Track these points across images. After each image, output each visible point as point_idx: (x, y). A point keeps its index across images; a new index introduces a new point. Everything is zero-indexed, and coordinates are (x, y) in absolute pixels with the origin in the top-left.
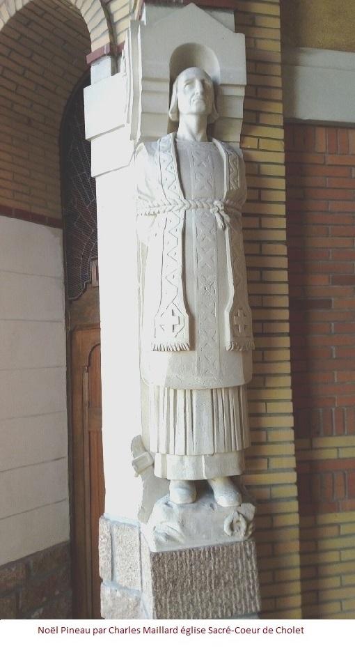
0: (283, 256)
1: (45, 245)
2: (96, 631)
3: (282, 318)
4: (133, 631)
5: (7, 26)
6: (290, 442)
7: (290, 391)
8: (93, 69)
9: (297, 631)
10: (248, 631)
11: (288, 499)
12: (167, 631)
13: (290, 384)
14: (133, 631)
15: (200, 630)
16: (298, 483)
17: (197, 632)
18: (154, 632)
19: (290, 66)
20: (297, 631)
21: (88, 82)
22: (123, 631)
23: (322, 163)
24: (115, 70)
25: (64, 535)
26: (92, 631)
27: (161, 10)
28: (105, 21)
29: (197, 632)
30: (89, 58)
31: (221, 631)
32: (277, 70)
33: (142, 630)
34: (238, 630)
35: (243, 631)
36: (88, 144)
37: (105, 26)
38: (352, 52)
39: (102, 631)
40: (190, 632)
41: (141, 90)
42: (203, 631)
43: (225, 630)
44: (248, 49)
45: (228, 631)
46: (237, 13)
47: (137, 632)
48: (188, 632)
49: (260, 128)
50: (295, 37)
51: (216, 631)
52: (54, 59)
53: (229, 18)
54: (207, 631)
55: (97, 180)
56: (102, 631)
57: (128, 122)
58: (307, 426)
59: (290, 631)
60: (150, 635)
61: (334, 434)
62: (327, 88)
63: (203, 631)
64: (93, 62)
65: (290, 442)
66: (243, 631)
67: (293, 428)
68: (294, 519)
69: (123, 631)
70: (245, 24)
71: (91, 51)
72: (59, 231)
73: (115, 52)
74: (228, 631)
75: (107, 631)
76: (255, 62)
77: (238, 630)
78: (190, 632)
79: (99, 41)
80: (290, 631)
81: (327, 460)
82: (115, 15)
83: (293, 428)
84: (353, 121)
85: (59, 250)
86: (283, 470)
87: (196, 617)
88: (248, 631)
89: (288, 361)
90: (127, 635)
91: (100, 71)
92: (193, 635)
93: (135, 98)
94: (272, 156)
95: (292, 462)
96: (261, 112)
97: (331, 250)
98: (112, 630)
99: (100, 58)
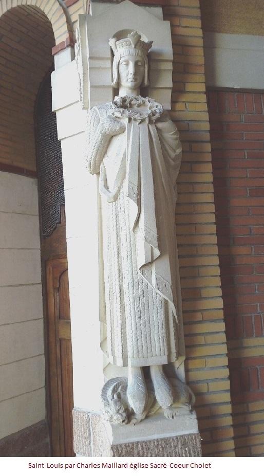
0: (211, 223)
1: (24, 189)
2: (68, 466)
3: (207, 160)
4: (95, 466)
6: (226, 391)
7: (218, 269)
8: (56, 57)
9: (206, 466)
10: (179, 466)
11: (225, 415)
12: (120, 466)
13: (215, 232)
14: (95, 466)
15: (144, 465)
16: (230, 377)
17: (142, 466)
18: (110, 466)
19: (210, 47)
20: (206, 466)
21: (54, 70)
22: (87, 466)
24: (73, 58)
26: (64, 466)
27: (102, 7)
28: (66, 25)
29: (142, 466)
30: (54, 51)
31: (159, 466)
32: (200, 52)
33: (101, 465)
34: (172, 466)
35: (176, 466)
37: (65, 28)
38: (259, 34)
39: (71, 466)
40: (137, 467)
41: (88, 56)
42: (146, 466)
43: (162, 466)
44: (174, 35)
45: (165, 466)
46: (163, 7)
47: (97, 466)
48: (135, 467)
49: (187, 95)
50: (210, 25)
51: (156, 466)
53: (159, 11)
54: (149, 466)
55: (58, 115)
56: (71, 466)
58: (235, 333)
59: (200, 466)
60: (107, 469)
61: (254, 336)
62: (239, 62)
63: (146, 466)
64: (56, 54)
65: (226, 391)
66: (176, 466)
68: (229, 421)
69: (87, 466)
70: (169, 14)
71: (55, 45)
72: (36, 180)
73: (72, 42)
74: (165, 466)
75: (75, 466)
76: (179, 44)
77: (172, 466)
78: (137, 467)
79: (60, 34)
80: (200, 466)
81: (247, 358)
84: (263, 87)
86: (215, 321)
88: (179, 466)
89: (214, 213)
90: (91, 469)
91: (62, 59)
92: (139, 469)
93: (84, 74)
94: (196, 110)
95: (225, 361)
96: (185, 82)
97: (248, 170)
98: (79, 465)
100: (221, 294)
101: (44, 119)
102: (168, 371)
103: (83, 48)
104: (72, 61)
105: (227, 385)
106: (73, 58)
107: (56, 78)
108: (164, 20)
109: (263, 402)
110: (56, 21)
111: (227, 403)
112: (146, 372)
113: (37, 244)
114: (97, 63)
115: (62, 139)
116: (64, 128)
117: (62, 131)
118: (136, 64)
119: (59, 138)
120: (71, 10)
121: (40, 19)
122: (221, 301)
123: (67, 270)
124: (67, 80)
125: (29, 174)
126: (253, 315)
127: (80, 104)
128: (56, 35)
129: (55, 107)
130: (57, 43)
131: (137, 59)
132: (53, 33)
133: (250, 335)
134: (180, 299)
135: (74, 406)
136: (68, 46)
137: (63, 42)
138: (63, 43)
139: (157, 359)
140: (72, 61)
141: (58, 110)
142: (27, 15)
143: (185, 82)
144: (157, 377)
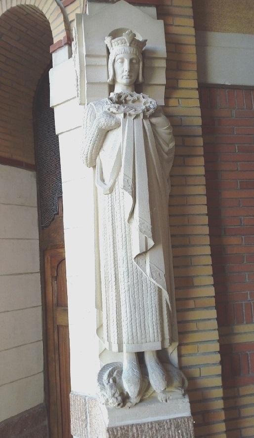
0: (203, 215)
1: (23, 182)
3: (199, 154)
5: (4, 14)
6: (218, 375)
7: (210, 258)
8: (54, 55)
13: (207, 223)
16: (222, 363)
19: (202, 45)
21: (52, 67)
23: (236, 169)
24: (70, 56)
25: (35, 397)
27: (98, 6)
28: (63, 24)
30: (51, 49)
32: (193, 50)
36: (52, 110)
37: (63, 27)
41: (85, 54)
44: (167, 34)
46: (157, 7)
49: (180, 91)
50: (202, 24)
52: (30, 45)
53: (153, 10)
55: (56, 111)
57: (78, 97)
58: (226, 320)
64: (54, 52)
65: (218, 375)
67: (207, 215)
68: (220, 404)
70: (163, 14)
71: (53, 43)
72: (35, 173)
73: (69, 41)
76: (172, 42)
79: (58, 33)
82: (68, 16)
83: (212, 276)
85: (34, 181)
86: (207, 308)
87: (128, 133)
89: (206, 205)
91: (59, 57)
93: (81, 71)
94: (189, 106)
95: (216, 347)
96: (178, 79)
99: (56, 50)
100: (212, 283)
101: (42, 115)
102: (162, 356)
103: (80, 46)
104: (69, 58)
105: (218, 369)
106: (70, 56)
107: (54, 75)
108: (158, 19)
109: (253, 386)
110: (54, 20)
111: (218, 387)
112: (140, 357)
113: (36, 234)
114: (94, 61)
115: (60, 134)
116: (61, 123)
117: (60, 126)
118: (131, 62)
119: (57, 132)
120: (69, 10)
121: (38, 18)
122: (213, 289)
123: (65, 259)
124: (64, 77)
125: (28, 167)
126: (243, 303)
127: (78, 99)
128: (54, 33)
129: (53, 102)
130: (55, 41)
131: (132, 57)
132: (51, 31)
133: (240, 322)
134: (174, 287)
135: (72, 390)
136: (65, 44)
137: (61, 41)
138: (61, 41)
139: (151, 345)
140: (69, 58)
141: (56, 106)
142: (26, 14)
143: (178, 79)
144: (151, 363)
